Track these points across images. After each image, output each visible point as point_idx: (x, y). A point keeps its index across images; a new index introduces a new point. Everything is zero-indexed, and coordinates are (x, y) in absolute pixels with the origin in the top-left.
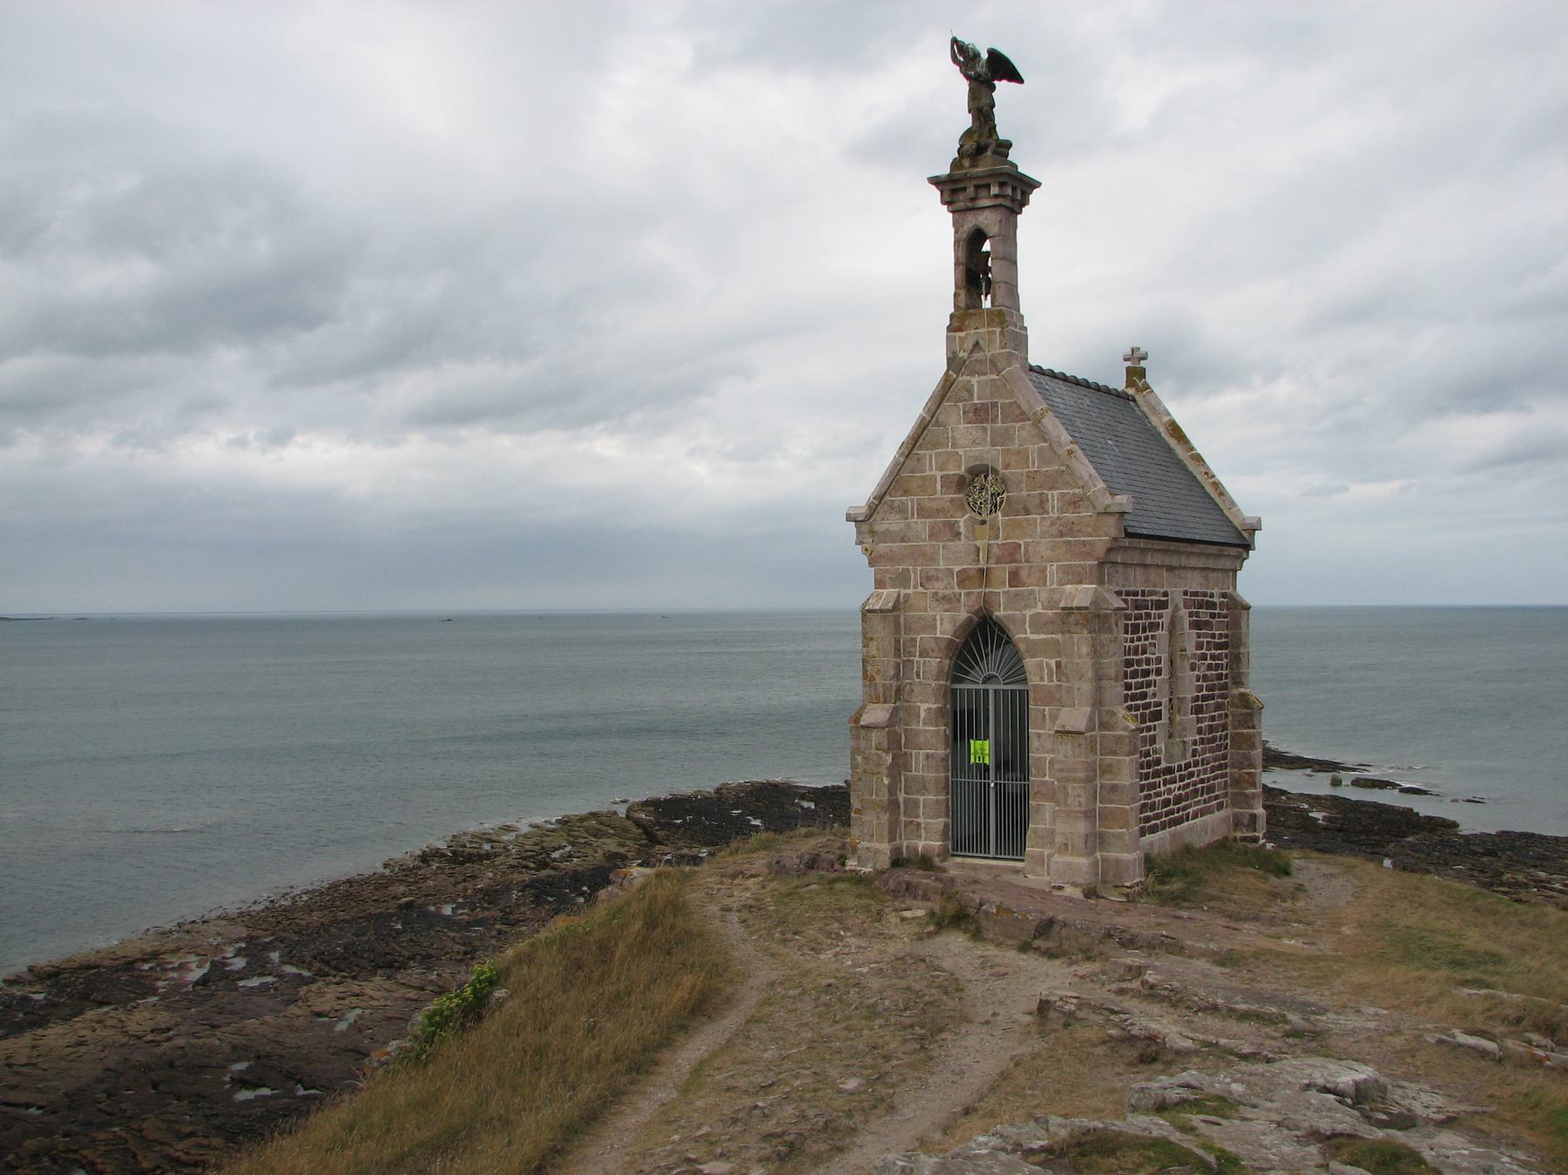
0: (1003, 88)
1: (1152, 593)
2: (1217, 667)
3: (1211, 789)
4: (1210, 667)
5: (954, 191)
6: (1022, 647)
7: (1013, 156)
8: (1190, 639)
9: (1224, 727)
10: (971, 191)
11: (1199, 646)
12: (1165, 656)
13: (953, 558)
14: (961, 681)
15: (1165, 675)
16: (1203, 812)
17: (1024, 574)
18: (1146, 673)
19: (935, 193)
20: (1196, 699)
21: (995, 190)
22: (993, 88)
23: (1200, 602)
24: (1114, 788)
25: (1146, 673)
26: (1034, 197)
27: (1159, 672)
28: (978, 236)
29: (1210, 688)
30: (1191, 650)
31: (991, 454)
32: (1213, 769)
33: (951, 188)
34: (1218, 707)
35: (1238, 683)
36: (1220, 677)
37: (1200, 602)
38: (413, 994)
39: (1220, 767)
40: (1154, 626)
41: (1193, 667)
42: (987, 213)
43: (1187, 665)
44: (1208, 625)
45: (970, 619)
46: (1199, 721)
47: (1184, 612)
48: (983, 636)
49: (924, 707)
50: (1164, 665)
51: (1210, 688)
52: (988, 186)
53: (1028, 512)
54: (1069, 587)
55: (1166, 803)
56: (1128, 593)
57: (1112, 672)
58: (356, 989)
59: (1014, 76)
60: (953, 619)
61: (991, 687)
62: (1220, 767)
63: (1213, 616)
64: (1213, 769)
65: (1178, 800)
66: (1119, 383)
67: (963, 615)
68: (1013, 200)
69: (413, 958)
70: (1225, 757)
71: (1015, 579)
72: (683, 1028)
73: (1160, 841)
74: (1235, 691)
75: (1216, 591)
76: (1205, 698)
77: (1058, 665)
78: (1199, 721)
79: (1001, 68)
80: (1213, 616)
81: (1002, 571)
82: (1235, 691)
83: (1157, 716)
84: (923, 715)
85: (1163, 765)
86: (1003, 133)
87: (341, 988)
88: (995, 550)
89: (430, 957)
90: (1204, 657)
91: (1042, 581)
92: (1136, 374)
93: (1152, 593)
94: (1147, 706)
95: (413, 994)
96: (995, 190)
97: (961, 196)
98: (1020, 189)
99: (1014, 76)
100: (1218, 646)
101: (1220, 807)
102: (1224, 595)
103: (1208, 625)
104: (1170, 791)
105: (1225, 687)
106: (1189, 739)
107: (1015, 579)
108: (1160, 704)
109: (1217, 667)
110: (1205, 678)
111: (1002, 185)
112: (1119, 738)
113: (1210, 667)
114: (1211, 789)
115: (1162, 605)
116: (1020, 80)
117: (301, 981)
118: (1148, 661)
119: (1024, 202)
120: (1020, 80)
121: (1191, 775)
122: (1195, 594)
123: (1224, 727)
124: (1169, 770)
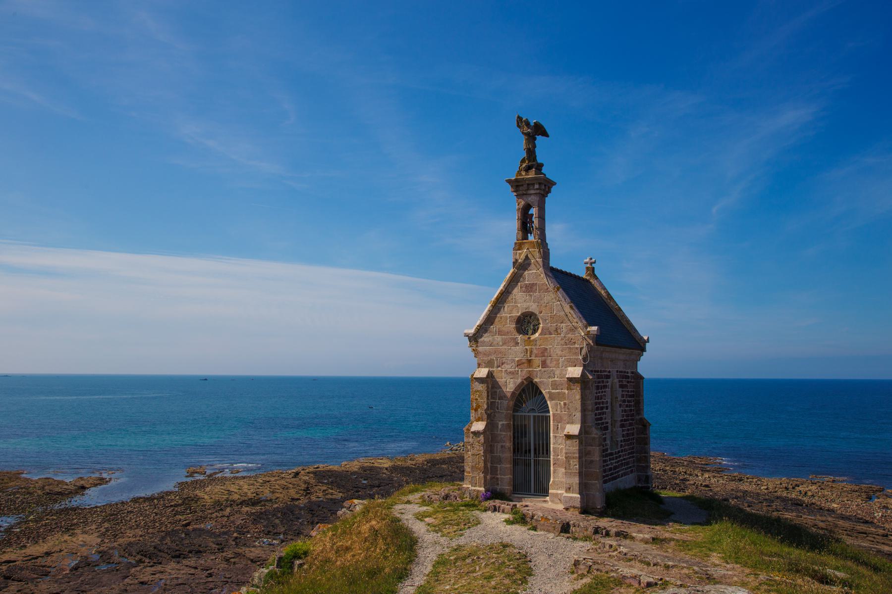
0: (540, 139)
1: (605, 371)
2: (630, 406)
3: (628, 463)
4: (627, 406)
5: (517, 186)
6: (547, 396)
7: (544, 170)
8: (619, 392)
9: (633, 434)
10: (525, 186)
11: (623, 396)
12: (609, 400)
13: (517, 353)
14: (517, 411)
15: (609, 410)
16: (625, 474)
17: (548, 362)
18: (602, 408)
19: (509, 186)
20: (622, 421)
21: (537, 186)
22: (535, 139)
23: (623, 375)
24: (592, 462)
25: (602, 408)
26: (554, 189)
27: (607, 408)
28: (527, 207)
29: (627, 416)
30: (620, 398)
31: (533, 308)
32: (629, 454)
33: (517, 185)
34: (631, 424)
35: (639, 414)
36: (631, 410)
37: (623, 375)
38: (192, 571)
39: (631, 453)
40: (605, 387)
41: (620, 405)
42: (533, 197)
43: (618, 405)
44: (626, 386)
45: (522, 383)
46: (623, 431)
47: (616, 380)
48: (530, 390)
49: (500, 423)
50: (609, 405)
51: (627, 416)
52: (533, 184)
53: (550, 334)
54: (569, 369)
55: (610, 469)
56: (595, 371)
57: (590, 408)
58: (162, 569)
59: (545, 134)
60: (515, 383)
61: (532, 414)
62: (631, 453)
63: (628, 382)
64: (629, 454)
65: (615, 468)
66: (583, 274)
67: (519, 381)
68: (544, 190)
69: (190, 552)
70: (633, 448)
71: (544, 364)
72: (411, 562)
73: (610, 486)
74: (638, 417)
75: (629, 371)
76: (625, 420)
77: (565, 404)
78: (623, 431)
79: (539, 130)
80: (628, 382)
81: (537, 361)
82: (638, 417)
83: (606, 428)
84: (500, 427)
85: (609, 451)
86: (539, 160)
87: (153, 569)
88: (535, 351)
89: (200, 552)
90: (624, 401)
91: (557, 366)
92: (591, 271)
93: (605, 371)
94: (603, 423)
95: (192, 571)
96: (537, 186)
97: (521, 188)
98: (546, 186)
99: (545, 134)
100: (631, 396)
101: (632, 472)
102: (632, 373)
103: (626, 386)
104: (612, 464)
105: (633, 415)
106: (619, 439)
107: (544, 364)
108: (607, 423)
109: (630, 406)
110: (625, 411)
111: (540, 184)
112: (594, 438)
113: (627, 406)
114: (628, 463)
115: (608, 377)
116: (547, 136)
117: (130, 566)
118: (603, 403)
119: (549, 192)
120: (547, 136)
121: (620, 456)
122: (621, 372)
123: (633, 434)
124: (611, 454)
